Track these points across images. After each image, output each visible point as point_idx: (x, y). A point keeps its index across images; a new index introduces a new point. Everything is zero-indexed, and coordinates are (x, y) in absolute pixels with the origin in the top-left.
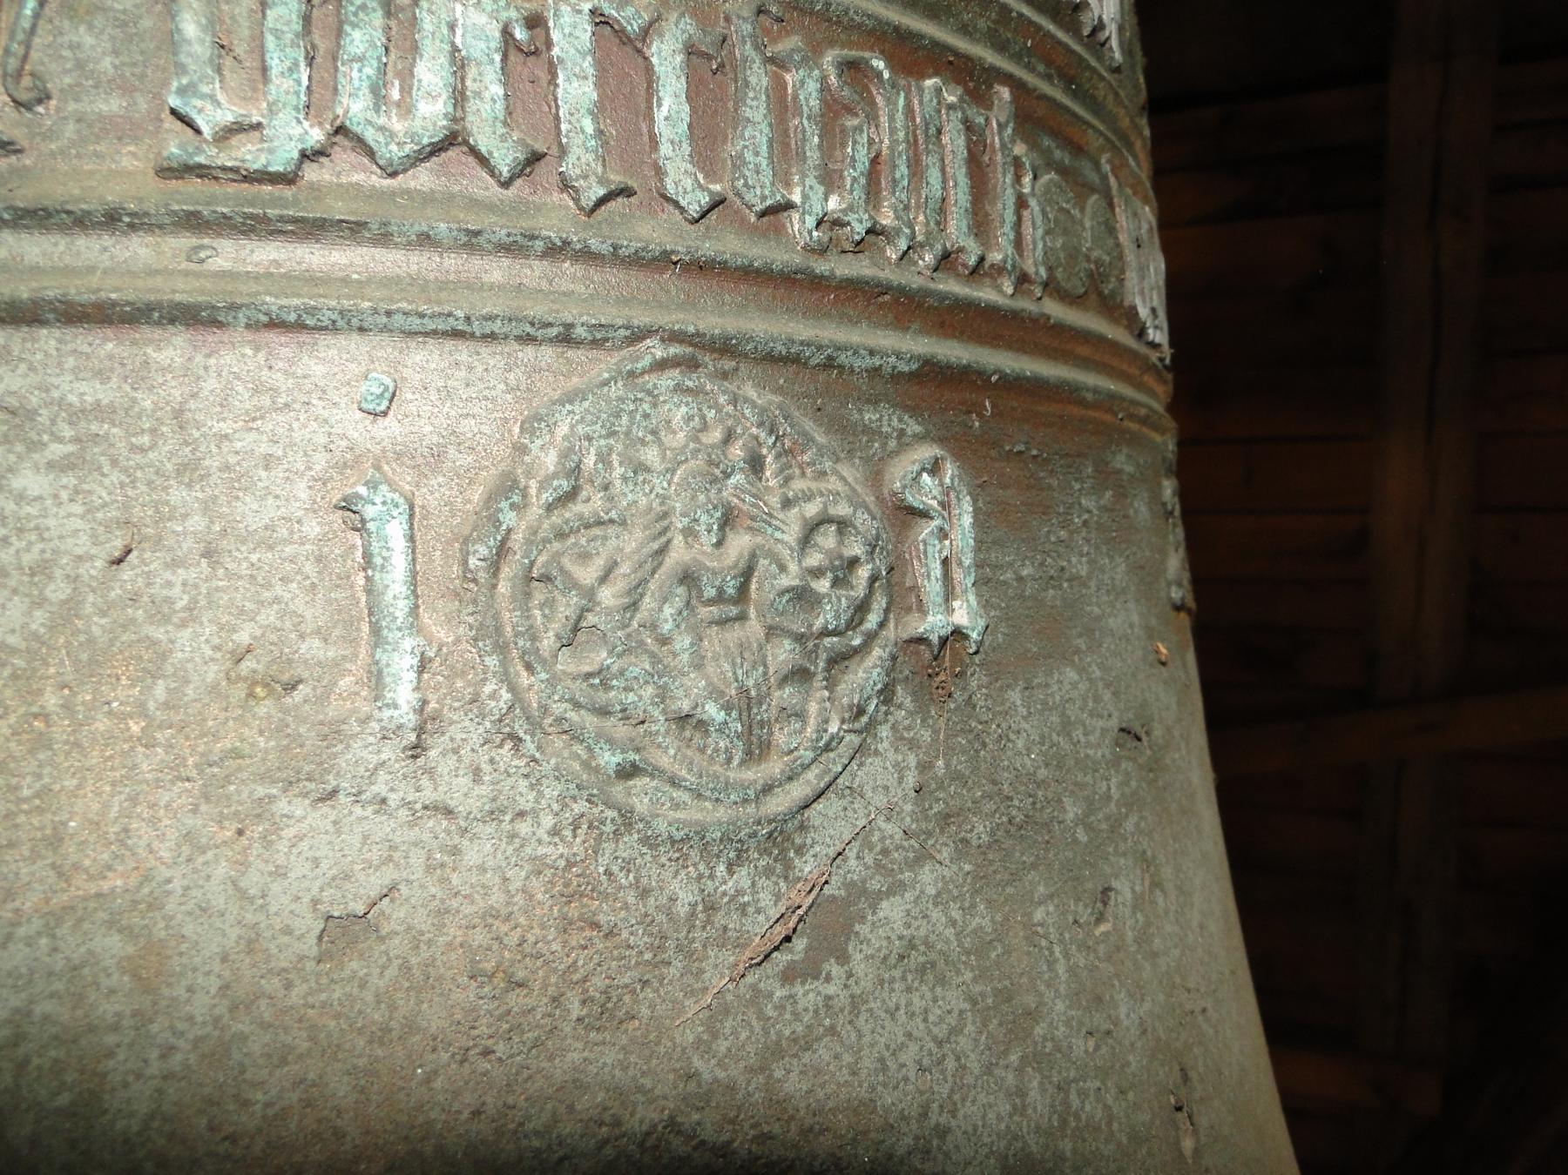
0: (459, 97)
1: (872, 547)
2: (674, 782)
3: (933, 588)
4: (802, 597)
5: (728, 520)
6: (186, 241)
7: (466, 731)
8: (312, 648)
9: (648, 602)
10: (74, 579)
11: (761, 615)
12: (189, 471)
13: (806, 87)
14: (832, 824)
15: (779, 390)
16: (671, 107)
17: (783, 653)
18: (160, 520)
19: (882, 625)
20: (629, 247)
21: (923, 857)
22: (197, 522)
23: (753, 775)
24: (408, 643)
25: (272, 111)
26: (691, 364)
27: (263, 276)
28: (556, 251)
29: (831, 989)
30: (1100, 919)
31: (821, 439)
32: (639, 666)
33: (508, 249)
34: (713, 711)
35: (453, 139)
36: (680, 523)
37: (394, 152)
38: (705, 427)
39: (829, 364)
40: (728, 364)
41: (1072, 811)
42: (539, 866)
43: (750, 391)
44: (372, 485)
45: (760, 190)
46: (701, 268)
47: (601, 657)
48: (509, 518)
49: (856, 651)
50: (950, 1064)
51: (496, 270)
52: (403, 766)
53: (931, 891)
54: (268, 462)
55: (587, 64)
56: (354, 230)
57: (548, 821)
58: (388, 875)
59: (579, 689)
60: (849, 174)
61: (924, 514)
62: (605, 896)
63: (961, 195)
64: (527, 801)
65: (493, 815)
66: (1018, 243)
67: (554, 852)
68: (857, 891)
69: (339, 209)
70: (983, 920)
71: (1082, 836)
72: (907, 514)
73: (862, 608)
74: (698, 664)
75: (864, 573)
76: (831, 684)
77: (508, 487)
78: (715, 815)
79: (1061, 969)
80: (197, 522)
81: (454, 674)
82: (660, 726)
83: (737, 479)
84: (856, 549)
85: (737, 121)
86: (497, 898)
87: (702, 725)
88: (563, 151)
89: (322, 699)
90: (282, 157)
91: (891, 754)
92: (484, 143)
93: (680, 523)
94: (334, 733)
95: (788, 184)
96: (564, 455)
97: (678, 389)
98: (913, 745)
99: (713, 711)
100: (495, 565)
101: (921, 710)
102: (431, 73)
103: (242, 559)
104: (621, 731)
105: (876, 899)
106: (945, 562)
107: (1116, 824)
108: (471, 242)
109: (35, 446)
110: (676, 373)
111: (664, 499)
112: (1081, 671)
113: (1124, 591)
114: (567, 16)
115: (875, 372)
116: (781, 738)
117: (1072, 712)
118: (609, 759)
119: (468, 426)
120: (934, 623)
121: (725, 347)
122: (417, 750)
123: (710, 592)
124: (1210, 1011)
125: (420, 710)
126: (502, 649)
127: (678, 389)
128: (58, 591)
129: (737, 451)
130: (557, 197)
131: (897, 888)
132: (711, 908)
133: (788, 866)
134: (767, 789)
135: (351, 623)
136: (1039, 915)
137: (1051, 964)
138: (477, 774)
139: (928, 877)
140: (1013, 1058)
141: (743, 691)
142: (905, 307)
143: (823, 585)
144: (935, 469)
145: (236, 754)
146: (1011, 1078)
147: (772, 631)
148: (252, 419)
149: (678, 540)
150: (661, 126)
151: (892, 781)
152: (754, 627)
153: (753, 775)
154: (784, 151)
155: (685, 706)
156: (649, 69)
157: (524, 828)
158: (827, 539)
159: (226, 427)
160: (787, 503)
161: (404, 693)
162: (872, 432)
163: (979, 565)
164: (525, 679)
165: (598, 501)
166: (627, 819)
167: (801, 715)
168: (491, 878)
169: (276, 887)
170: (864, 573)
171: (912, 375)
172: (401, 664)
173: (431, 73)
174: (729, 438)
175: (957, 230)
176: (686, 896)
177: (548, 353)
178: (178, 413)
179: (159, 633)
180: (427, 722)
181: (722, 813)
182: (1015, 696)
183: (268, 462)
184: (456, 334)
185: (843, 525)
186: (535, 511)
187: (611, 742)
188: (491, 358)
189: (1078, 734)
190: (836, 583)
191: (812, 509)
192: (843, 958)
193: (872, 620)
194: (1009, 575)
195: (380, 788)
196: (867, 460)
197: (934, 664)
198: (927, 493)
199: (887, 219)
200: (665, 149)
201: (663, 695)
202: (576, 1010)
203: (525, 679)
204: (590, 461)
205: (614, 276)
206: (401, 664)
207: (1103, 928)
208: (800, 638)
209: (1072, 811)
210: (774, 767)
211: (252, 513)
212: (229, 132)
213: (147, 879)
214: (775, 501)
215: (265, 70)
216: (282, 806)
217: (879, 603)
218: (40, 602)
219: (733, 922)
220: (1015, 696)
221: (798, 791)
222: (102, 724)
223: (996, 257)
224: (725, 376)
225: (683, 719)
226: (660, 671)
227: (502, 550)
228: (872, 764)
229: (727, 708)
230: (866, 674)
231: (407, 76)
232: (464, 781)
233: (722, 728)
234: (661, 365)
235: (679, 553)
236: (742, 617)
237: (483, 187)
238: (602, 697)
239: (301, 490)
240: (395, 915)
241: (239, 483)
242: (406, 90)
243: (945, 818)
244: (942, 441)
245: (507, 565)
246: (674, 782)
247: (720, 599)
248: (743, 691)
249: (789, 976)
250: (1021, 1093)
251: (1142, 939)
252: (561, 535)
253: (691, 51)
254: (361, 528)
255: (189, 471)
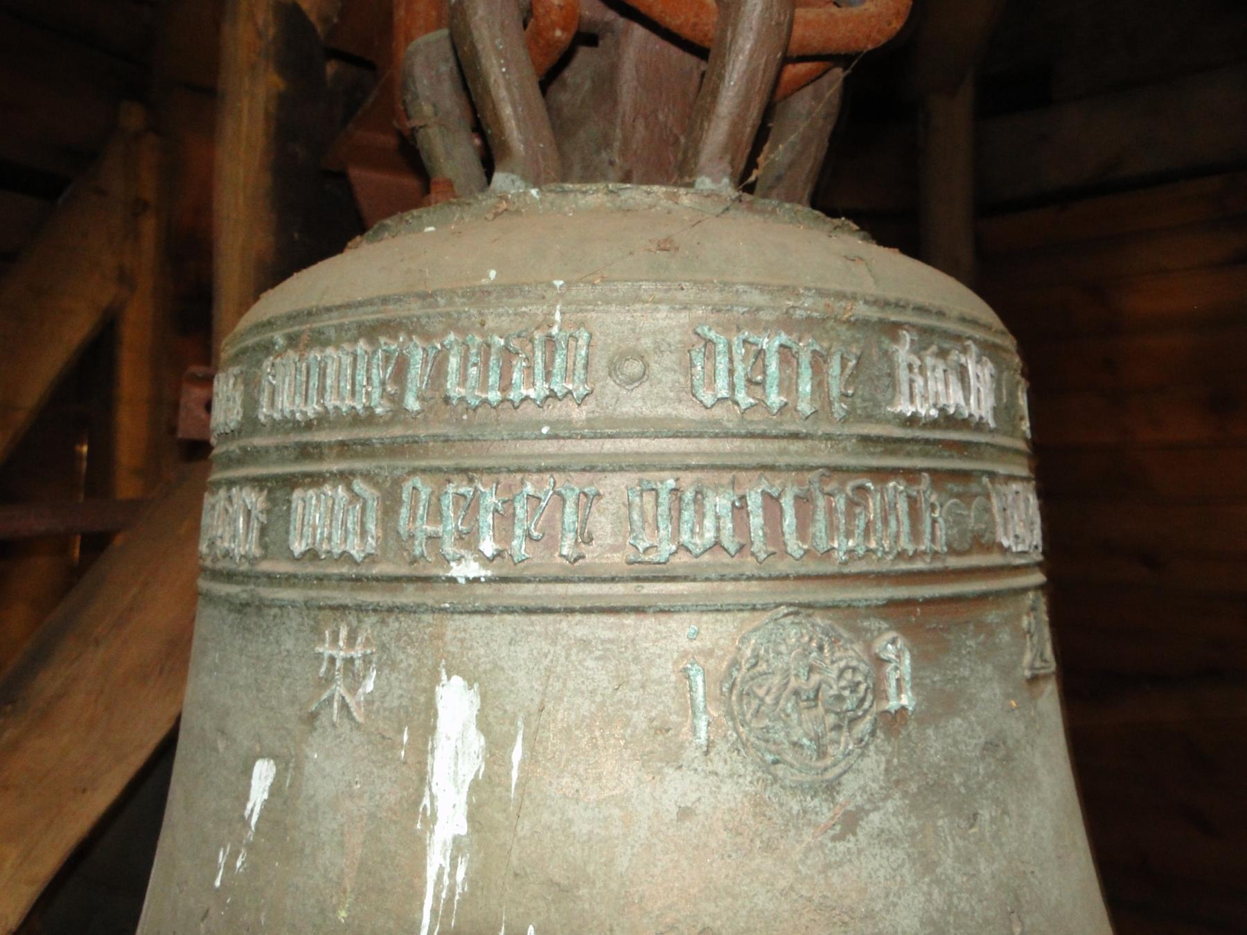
0: (718, 529)
1: (866, 677)
2: (792, 766)
3: (892, 690)
4: (839, 698)
5: (811, 669)
6: (635, 584)
7: (722, 747)
8: (674, 718)
9: (782, 702)
10: (603, 695)
11: (823, 705)
12: (636, 660)
13: (840, 503)
14: (851, 784)
15: (830, 619)
16: (789, 521)
17: (831, 719)
18: (628, 676)
19: (871, 706)
20: (774, 573)
21: (886, 798)
22: (639, 676)
23: (821, 764)
24: (704, 717)
25: (660, 542)
26: (796, 614)
27: (658, 596)
28: (749, 579)
29: (850, 845)
30: (972, 826)
31: (846, 635)
32: (779, 725)
33: (736, 579)
34: (805, 741)
35: (717, 543)
36: (793, 672)
37: (698, 551)
38: (802, 636)
39: (849, 606)
40: (810, 611)
41: (958, 780)
42: (746, 794)
43: (819, 620)
44: (692, 664)
45: (823, 545)
46: (800, 578)
47: (766, 722)
48: (735, 674)
49: (860, 717)
50: (898, 879)
51: (730, 587)
52: (702, 758)
53: (891, 810)
54: (660, 656)
55: (760, 511)
56: (686, 579)
57: (749, 779)
58: (698, 794)
59: (759, 732)
60: (857, 532)
61: (889, 661)
62: (768, 806)
63: (906, 528)
64: (742, 771)
65: (731, 776)
66: (933, 540)
67: (751, 789)
68: (860, 809)
69: (681, 572)
70: (914, 823)
71: (963, 790)
72: (880, 662)
73: (862, 700)
74: (800, 724)
75: (863, 687)
76: (850, 730)
77: (735, 663)
78: (807, 778)
79: (951, 845)
80: (639, 676)
81: (718, 728)
82: (787, 745)
83: (814, 654)
84: (860, 678)
85: (813, 521)
86: (732, 804)
87: (802, 746)
88: (752, 543)
89: (676, 735)
90: (664, 556)
91: (875, 757)
92: (726, 544)
93: (793, 672)
94: (681, 746)
95: (833, 540)
96: (753, 650)
97: (793, 623)
98: (884, 753)
99: (805, 741)
100: (731, 691)
101: (888, 739)
102: (709, 523)
103: (653, 688)
104: (773, 748)
105: (867, 813)
106: (898, 680)
107: (981, 786)
108: (722, 578)
109: (591, 652)
110: (791, 617)
111: (787, 664)
112: (964, 719)
113: (991, 679)
114: (753, 495)
115: (868, 607)
116: (831, 750)
117: (959, 738)
118: (769, 758)
119: (722, 642)
120: (893, 705)
121: (809, 606)
122: (707, 753)
123: (804, 697)
124: (1037, 873)
125: (708, 740)
126: (733, 719)
127: (793, 623)
128: (599, 699)
129: (814, 644)
130: (750, 559)
131: (877, 809)
132: (805, 812)
133: (833, 798)
134: (826, 769)
135: (686, 710)
136: (940, 823)
137: (946, 843)
138: (726, 762)
139: (890, 806)
140: (927, 880)
141: (816, 733)
142: (881, 578)
143: (846, 693)
144: (893, 642)
145: (652, 752)
146: (925, 888)
147: (827, 711)
148: (655, 641)
149: (793, 679)
150: (786, 529)
151: (874, 766)
152: (821, 709)
153: (821, 764)
154: (832, 528)
155: (795, 739)
156: (781, 509)
157: (741, 780)
158: (848, 675)
159: (646, 645)
160: (833, 662)
161: (703, 734)
162: (867, 630)
163: (913, 678)
164: (741, 729)
165: (764, 666)
166: (776, 779)
167: (838, 742)
168: (730, 797)
169: (664, 796)
170: (863, 687)
171: (884, 606)
172: (702, 724)
173: (709, 523)
174: (811, 639)
175: (905, 543)
176: (796, 808)
177: (746, 614)
178: (633, 641)
179: (628, 712)
180: (710, 744)
181: (809, 778)
182: (930, 732)
183: (660, 656)
184: (718, 611)
185: (854, 669)
186: (744, 670)
187: (770, 752)
188: (728, 617)
189: (962, 747)
190: (852, 692)
191: (842, 664)
192: (855, 834)
193: (866, 705)
194: (928, 681)
195: (695, 765)
196: (865, 641)
197: (893, 722)
198: (890, 652)
199: (873, 545)
200: (787, 536)
201: (788, 734)
202: (758, 844)
203: (741, 729)
204: (762, 652)
205: (769, 584)
206: (702, 724)
207: (973, 830)
208: (837, 714)
209: (958, 780)
210: (829, 761)
211: (655, 673)
212: (646, 550)
213: (626, 791)
214: (828, 661)
215: (658, 528)
216: (666, 770)
217: (870, 697)
218: (594, 702)
219: (813, 817)
220: (930, 732)
221: (837, 770)
222: (612, 741)
223: (923, 548)
224: (809, 616)
225: (794, 744)
226: (787, 726)
227: (733, 684)
228: (867, 761)
229: (811, 740)
230: (864, 726)
231: (701, 524)
232: (722, 764)
233: (809, 747)
234: (786, 615)
235: (793, 683)
236: (816, 706)
237: (725, 559)
238: (767, 736)
239: (670, 666)
240: (701, 808)
241: (651, 663)
242: (701, 528)
243: (897, 782)
244: (897, 629)
245: (737, 690)
246: (792, 766)
247: (808, 699)
248: (816, 733)
249: (834, 839)
250: (930, 894)
251: (996, 836)
252: (752, 679)
253: (797, 498)
254: (688, 678)
255: (636, 660)
